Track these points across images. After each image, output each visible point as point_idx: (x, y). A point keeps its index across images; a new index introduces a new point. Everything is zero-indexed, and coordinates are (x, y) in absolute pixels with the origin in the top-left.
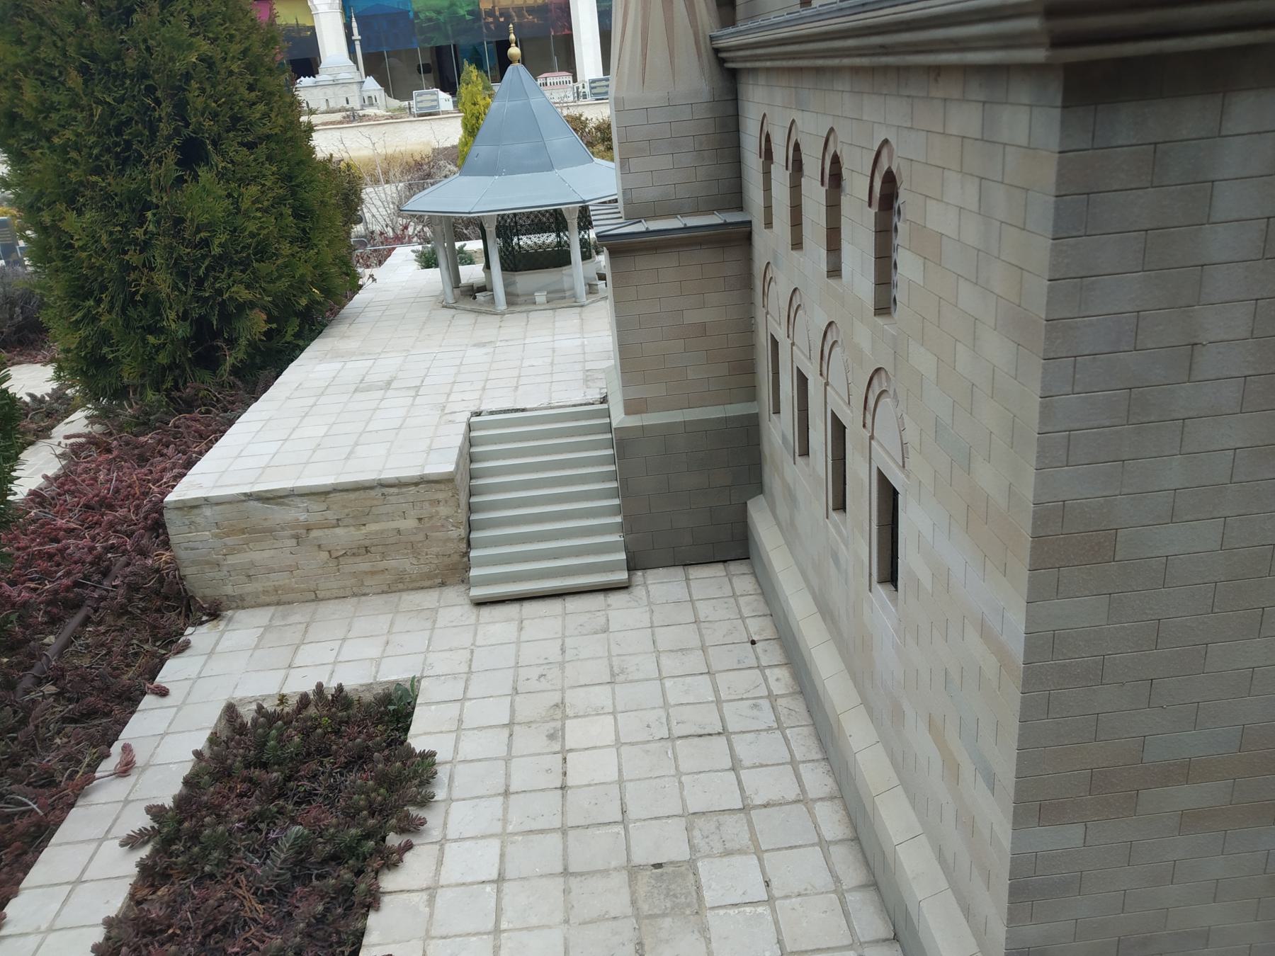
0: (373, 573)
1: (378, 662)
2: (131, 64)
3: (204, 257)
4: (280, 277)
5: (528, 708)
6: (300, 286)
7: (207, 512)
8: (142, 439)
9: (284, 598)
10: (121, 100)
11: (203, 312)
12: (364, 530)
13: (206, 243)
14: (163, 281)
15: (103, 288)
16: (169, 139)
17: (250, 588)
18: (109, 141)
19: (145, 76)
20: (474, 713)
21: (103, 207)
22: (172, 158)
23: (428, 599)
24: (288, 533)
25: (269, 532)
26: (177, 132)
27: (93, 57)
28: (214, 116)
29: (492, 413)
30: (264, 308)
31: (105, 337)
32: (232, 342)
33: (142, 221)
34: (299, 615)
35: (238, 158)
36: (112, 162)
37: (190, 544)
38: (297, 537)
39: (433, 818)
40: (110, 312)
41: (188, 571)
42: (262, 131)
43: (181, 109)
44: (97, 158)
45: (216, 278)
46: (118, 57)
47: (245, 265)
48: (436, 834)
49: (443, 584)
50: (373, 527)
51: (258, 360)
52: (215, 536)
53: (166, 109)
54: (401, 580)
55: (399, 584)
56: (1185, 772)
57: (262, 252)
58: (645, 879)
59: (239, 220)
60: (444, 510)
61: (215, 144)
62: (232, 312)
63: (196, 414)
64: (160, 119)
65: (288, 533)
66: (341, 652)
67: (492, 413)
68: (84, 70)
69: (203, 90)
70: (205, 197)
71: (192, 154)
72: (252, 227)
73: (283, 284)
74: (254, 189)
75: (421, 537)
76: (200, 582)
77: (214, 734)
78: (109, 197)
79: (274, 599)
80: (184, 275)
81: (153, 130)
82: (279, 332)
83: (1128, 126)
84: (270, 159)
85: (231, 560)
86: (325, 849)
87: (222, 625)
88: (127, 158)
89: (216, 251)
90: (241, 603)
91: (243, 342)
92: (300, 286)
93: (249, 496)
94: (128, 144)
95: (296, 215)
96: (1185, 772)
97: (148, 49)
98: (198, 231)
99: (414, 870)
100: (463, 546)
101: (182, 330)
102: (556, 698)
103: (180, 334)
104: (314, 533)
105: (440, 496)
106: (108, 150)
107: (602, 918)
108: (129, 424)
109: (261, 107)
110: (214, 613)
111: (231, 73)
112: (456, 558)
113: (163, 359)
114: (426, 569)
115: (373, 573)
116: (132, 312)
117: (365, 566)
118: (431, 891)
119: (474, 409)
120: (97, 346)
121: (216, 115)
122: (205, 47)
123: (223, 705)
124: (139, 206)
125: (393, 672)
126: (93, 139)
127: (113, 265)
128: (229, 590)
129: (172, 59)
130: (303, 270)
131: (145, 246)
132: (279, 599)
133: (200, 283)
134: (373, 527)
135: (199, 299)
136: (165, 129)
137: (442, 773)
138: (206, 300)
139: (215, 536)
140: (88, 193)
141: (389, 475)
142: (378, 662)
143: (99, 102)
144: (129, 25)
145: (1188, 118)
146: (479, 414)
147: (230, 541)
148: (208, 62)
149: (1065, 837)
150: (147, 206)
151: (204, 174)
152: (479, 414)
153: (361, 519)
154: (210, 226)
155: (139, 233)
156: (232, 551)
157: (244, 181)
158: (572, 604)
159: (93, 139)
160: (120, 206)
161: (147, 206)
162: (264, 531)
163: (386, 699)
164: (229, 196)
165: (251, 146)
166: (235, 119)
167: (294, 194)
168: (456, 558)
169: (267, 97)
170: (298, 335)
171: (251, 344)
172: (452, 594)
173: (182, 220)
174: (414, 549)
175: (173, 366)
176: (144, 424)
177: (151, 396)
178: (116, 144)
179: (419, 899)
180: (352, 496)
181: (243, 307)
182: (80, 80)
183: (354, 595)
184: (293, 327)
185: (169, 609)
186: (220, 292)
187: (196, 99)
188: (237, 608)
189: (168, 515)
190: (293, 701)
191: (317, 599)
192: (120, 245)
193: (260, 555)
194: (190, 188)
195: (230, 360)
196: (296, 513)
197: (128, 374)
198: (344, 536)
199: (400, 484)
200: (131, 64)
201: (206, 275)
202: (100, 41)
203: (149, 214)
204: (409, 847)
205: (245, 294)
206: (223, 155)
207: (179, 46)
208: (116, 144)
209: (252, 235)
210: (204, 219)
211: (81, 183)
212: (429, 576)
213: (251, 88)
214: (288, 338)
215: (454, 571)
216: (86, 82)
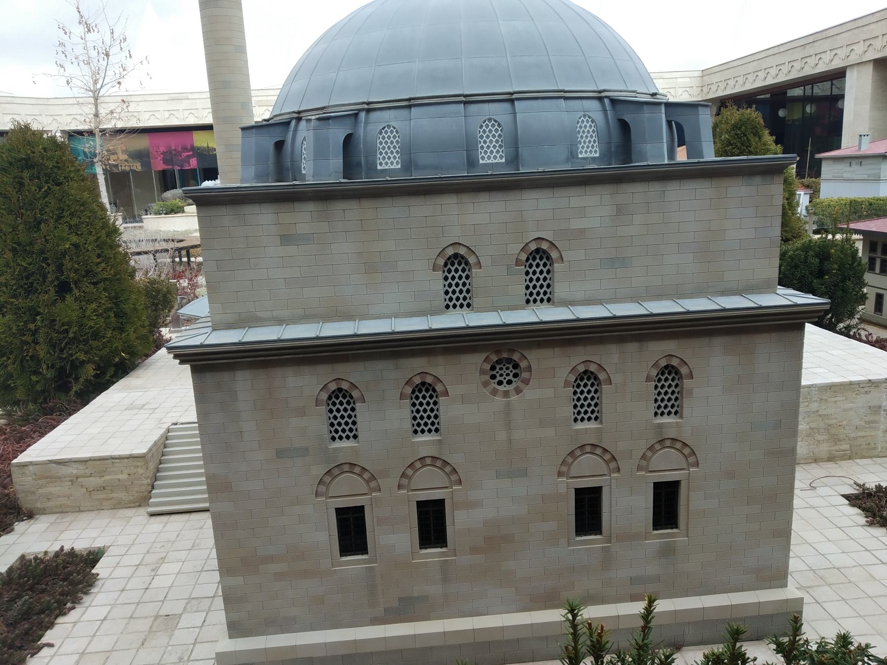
0: (107, 499)
1: (95, 539)
2: (36, 247)
3: (65, 338)
4: (104, 348)
5: (150, 559)
6: (115, 352)
7: (31, 468)
8: (23, 428)
9: (64, 510)
10: (30, 264)
11: (62, 364)
12: (103, 479)
13: (67, 331)
14: (42, 351)
15: (11, 353)
16: (52, 282)
17: (51, 504)
18: (22, 283)
19: (43, 253)
20: (126, 560)
21: (16, 313)
22: (52, 291)
23: (129, 512)
24: (67, 479)
25: (59, 478)
26: (57, 278)
27: (19, 244)
28: (76, 271)
29: (182, 424)
30: (94, 362)
31: (10, 376)
32: (77, 379)
33: (35, 320)
34: (69, 518)
35: (87, 290)
36: (23, 292)
37: (21, 483)
38: (72, 481)
39: (86, 599)
40: (14, 364)
41: (19, 496)
42: (100, 277)
43: (60, 268)
44: (15, 290)
45: (70, 349)
46: (31, 244)
47: (86, 342)
48: (87, 604)
49: (140, 506)
50: (107, 478)
51: (90, 389)
52: (34, 479)
53: (52, 268)
54: (120, 503)
55: (119, 505)
56: (271, 559)
57: (96, 336)
58: (160, 620)
59: (85, 321)
60: (140, 471)
61: (76, 283)
62: (76, 366)
63: (54, 416)
64: (49, 273)
65: (67, 479)
66: (77, 535)
67: (182, 424)
68: (14, 250)
69: (72, 259)
70: (69, 309)
71: (63, 288)
72: (92, 324)
73: (105, 352)
74: (94, 306)
75: (130, 483)
76: (26, 502)
77: (12, 567)
78: (19, 309)
79: (60, 510)
80: (53, 346)
81: (45, 277)
82: (104, 373)
83: (210, 378)
84: (105, 289)
85: (40, 491)
86: (38, 607)
87: (32, 521)
88: (30, 290)
89: (71, 335)
90: (43, 512)
91: (82, 380)
92: (115, 352)
93: (51, 462)
94: (32, 283)
95: (117, 316)
96: (271, 559)
97: (46, 240)
98: (63, 325)
99: (73, 616)
100: (150, 488)
101: (50, 374)
102: (163, 555)
103: (49, 376)
104: (80, 480)
105: (139, 464)
106: (21, 287)
107: (136, 632)
108: (19, 420)
109: (103, 265)
110: (30, 516)
111: (88, 250)
112: (146, 493)
113: (38, 388)
114: (132, 498)
115: (107, 499)
116: (25, 364)
117: (103, 496)
118: (75, 623)
119: (174, 421)
120: (7, 379)
121: (78, 270)
122: (74, 239)
123: (19, 555)
124: (34, 313)
125: (98, 544)
126: (14, 282)
127: (17, 341)
128: (39, 505)
129: (58, 245)
130: (118, 344)
131: (35, 333)
132: (62, 511)
133: (62, 350)
134: (107, 478)
135: (61, 358)
136: (50, 277)
137: (99, 583)
138: (64, 359)
139: (34, 479)
140: (9, 306)
141: (116, 453)
142: (95, 539)
143: (19, 265)
144: (39, 230)
145: (225, 376)
146: (176, 424)
147: (41, 482)
148: (76, 246)
149: (238, 581)
150: (38, 314)
151: (69, 298)
152: (176, 424)
153: (101, 474)
154: (69, 324)
155: (32, 326)
156: (41, 487)
157: (89, 302)
158: (194, 516)
159: (14, 282)
160: (24, 313)
161: (38, 314)
162: (60, 478)
163: (90, 553)
164: (81, 308)
165: (95, 284)
166: (88, 272)
167: (117, 305)
168: (146, 493)
169: (106, 260)
170: (112, 377)
171: (86, 380)
172: (143, 511)
173: (55, 320)
174: (126, 489)
175: (43, 392)
176: (25, 420)
177: (31, 406)
178: (26, 284)
179: (69, 626)
180: (98, 463)
181: (83, 363)
182: (11, 254)
183: (98, 510)
184: (111, 371)
185: (11, 514)
186: (71, 355)
187: (67, 263)
188: (42, 514)
189: (13, 469)
190: (51, 555)
191: (80, 511)
192: (22, 331)
193: (53, 489)
194: (60, 305)
195: (74, 389)
196: (72, 470)
197: (20, 394)
198: (94, 481)
199: (120, 458)
200: (36, 247)
201: (65, 347)
202: (23, 238)
203: (38, 318)
204: (74, 608)
205: (82, 357)
206: (79, 289)
207: (62, 239)
208: (26, 284)
209: (91, 327)
210: (66, 320)
211: (6, 302)
212: (133, 502)
213: (99, 256)
214: (107, 378)
215: (142, 501)
216: (14, 255)
